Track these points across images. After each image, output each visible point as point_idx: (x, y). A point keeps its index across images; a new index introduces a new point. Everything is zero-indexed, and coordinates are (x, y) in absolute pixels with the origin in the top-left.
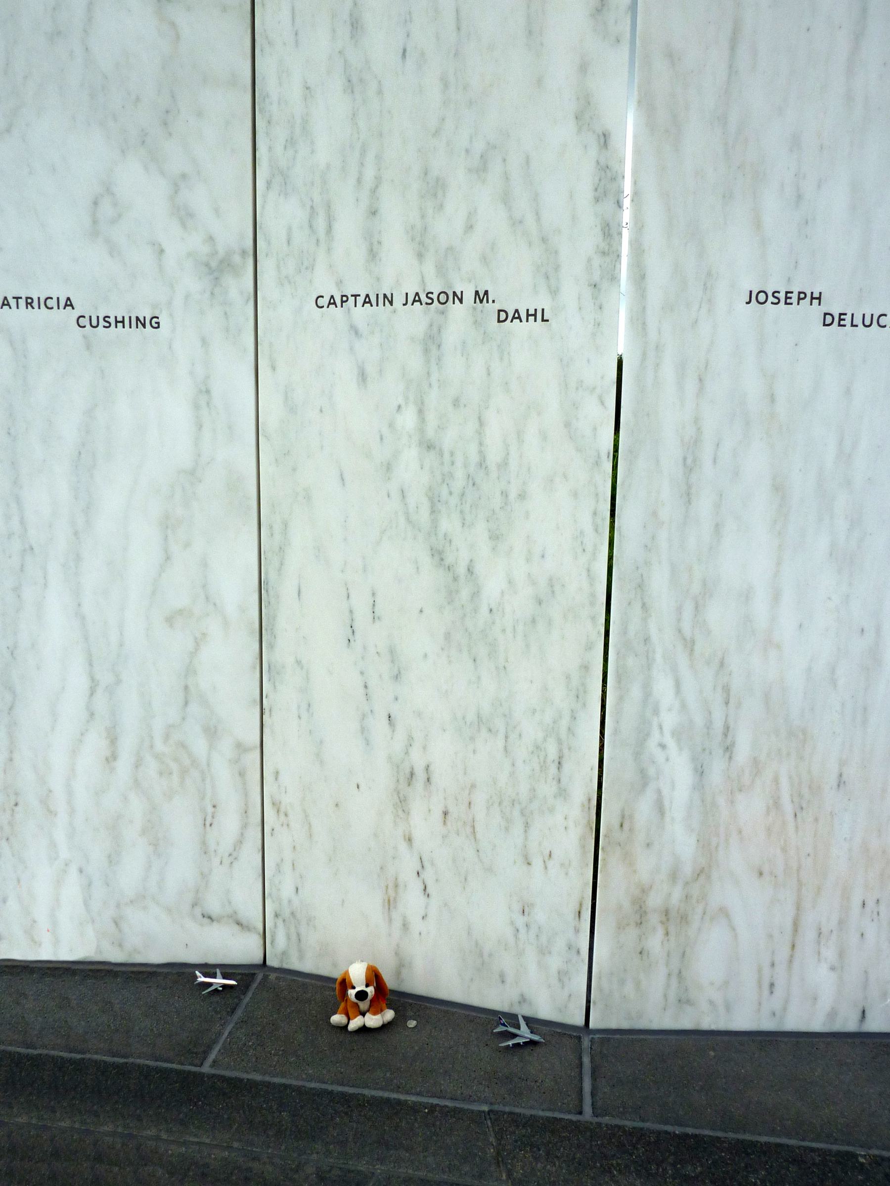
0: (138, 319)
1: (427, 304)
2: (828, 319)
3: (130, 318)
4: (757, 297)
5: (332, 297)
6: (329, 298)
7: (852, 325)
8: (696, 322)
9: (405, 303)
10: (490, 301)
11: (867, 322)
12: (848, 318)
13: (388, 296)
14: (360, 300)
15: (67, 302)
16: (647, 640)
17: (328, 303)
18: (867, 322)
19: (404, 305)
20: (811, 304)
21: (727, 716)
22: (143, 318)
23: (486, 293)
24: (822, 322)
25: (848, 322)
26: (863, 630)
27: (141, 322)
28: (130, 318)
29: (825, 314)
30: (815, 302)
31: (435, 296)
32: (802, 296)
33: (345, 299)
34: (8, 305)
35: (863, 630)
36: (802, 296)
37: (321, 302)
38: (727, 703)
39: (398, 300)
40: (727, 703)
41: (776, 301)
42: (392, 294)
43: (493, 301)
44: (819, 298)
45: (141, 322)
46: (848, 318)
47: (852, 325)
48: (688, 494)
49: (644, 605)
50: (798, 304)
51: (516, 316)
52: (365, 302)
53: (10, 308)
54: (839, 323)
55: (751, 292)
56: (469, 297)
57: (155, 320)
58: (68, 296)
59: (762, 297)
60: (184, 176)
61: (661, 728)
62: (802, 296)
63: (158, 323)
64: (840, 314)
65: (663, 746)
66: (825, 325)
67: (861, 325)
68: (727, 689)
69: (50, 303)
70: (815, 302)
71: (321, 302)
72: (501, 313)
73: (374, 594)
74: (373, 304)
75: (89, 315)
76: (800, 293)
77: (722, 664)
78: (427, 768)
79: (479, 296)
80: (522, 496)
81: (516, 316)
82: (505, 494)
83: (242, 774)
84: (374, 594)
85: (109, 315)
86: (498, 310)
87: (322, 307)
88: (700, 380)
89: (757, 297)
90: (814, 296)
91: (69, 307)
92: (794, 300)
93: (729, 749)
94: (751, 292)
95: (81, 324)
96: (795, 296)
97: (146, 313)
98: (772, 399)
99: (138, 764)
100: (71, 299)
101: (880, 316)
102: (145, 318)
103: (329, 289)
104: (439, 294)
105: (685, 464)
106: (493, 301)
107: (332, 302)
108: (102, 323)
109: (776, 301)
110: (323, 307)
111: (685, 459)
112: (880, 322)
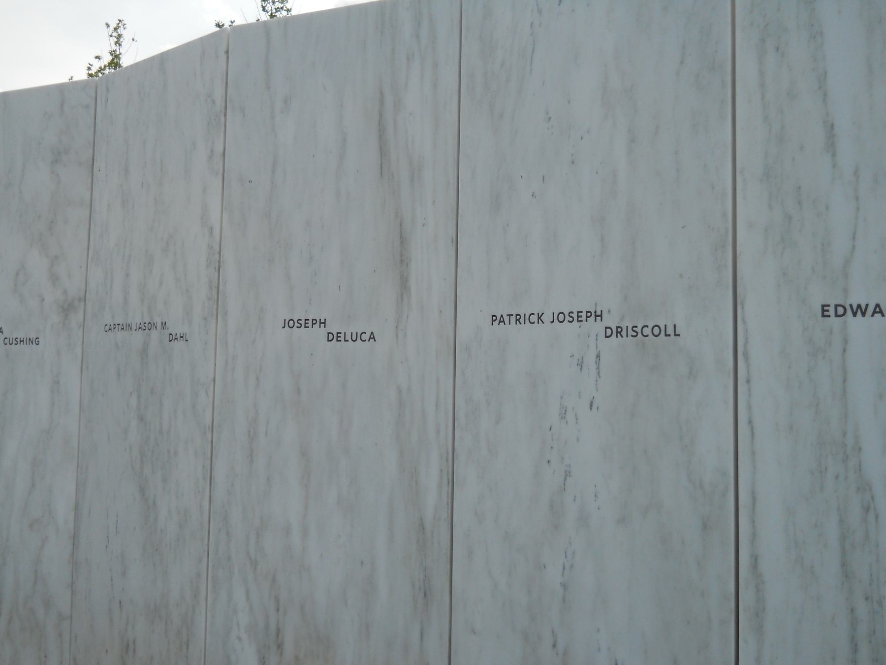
0: (30, 339)
1: (632, 336)
2: (332, 337)
3: (27, 338)
4: (289, 324)
7: (345, 341)
8: (254, 341)
9: (552, 321)
11: (354, 339)
12: (342, 335)
14: (120, 327)
15: (875, 309)
16: (229, 558)
17: (311, 324)
18: (354, 339)
19: (552, 322)
21: (278, 621)
22: (626, 328)
24: (604, 335)
25: (342, 338)
26: (362, 562)
27: (31, 341)
28: (27, 338)
29: (606, 328)
30: (599, 318)
31: (639, 330)
32: (314, 322)
33: (494, 318)
34: (503, 321)
35: (362, 562)
36: (314, 322)
38: (278, 610)
39: (547, 318)
40: (278, 610)
41: (571, 319)
42: (525, 314)
44: (324, 323)
45: (31, 341)
46: (342, 335)
47: (345, 341)
48: (251, 456)
49: (228, 533)
50: (587, 321)
53: (505, 324)
54: (337, 339)
55: (285, 320)
56: (159, 325)
58: (850, 304)
59: (291, 323)
60: (56, 257)
61: (238, 624)
62: (589, 314)
64: (338, 333)
65: (239, 639)
66: (328, 341)
67: (8, 344)
68: (277, 599)
69: (647, 331)
70: (599, 318)
72: (607, 329)
73: (117, 516)
76: (313, 320)
77: (274, 580)
78: (134, 641)
80: (176, 453)
82: (169, 451)
83: (60, 636)
84: (117, 516)
87: (534, 323)
88: (257, 379)
89: (289, 324)
90: (321, 322)
92: (310, 324)
93: (280, 646)
94: (285, 320)
96: (310, 322)
97: (33, 336)
98: (299, 391)
99: (10, 621)
101: (362, 333)
103: (109, 321)
104: (293, 326)
105: (249, 435)
108: (631, 332)
109: (571, 319)
110: (365, 340)
111: (249, 431)
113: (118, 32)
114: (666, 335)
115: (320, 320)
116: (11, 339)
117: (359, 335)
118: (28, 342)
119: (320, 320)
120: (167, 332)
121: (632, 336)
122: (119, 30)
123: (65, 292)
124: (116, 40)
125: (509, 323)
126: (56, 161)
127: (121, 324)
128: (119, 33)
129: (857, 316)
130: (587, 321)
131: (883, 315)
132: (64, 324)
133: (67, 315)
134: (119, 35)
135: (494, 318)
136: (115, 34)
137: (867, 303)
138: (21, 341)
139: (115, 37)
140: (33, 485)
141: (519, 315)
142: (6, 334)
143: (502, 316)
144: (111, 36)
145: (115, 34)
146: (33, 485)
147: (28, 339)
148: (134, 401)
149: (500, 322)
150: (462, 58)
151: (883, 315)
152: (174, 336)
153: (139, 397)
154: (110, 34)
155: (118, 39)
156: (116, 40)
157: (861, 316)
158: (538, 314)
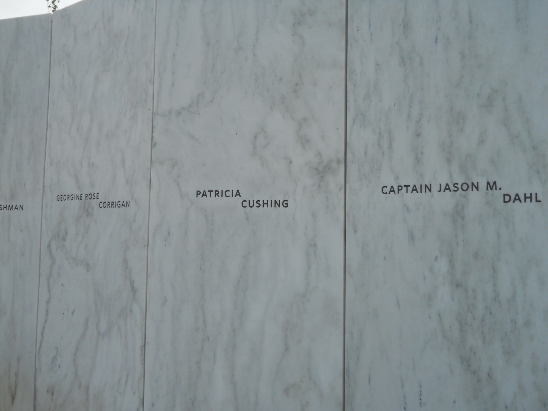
1: (454, 191)
3: (271, 201)
5: (392, 187)
6: (390, 187)
9: (439, 190)
10: (498, 188)
11: (251, 205)
13: (428, 186)
14: (410, 189)
15: (516, 197)
18: (251, 205)
19: (439, 191)
20: (197, 197)
23: (495, 183)
27: (277, 204)
30: (265, 202)
34: (206, 195)
37: (385, 190)
39: (435, 188)
42: (222, 191)
43: (500, 189)
45: (277, 204)
51: (392, 190)
52: (413, 190)
53: (207, 197)
56: (483, 186)
57: (285, 202)
60: (305, 120)
63: (287, 204)
67: (103, 207)
69: (228, 194)
71: (385, 190)
74: (418, 191)
75: (123, 201)
79: (21, 208)
81: (392, 190)
82: (514, 322)
85: (72, 194)
86: (288, 204)
87: (246, 207)
91: (415, 191)
94: (253, 201)
95: (384, 192)
97: (280, 198)
100: (394, 187)
102: (280, 201)
103: (390, 182)
106: (500, 189)
107: (392, 190)
112: (243, 205)
113: (54, 4)
114: (537, 201)
115: (267, 207)
116: (75, 199)
117: (117, 204)
118: (76, 197)
119: (267, 207)
120: (498, 194)
121: (454, 191)
122: (55, 3)
123: (319, 154)
124: (53, 9)
125: (210, 196)
126: (299, 24)
127: (412, 186)
128: (55, 5)
129: (486, 183)
130: (398, 193)
131: (240, 197)
132: (319, 186)
133: (322, 177)
134: (55, 6)
135: (198, 193)
136: (52, 5)
137: (541, 201)
138: (4, 207)
139: (52, 7)
140: (287, 349)
141: (218, 191)
142: (244, 197)
143: (204, 191)
144: (50, 7)
145: (52, 5)
146: (287, 349)
147: (273, 202)
148: (443, 266)
149: (203, 195)
150: (348, 9)
151: (240, 197)
152: (107, 204)
153: (451, 262)
154: (49, 6)
155: (54, 8)
156: (53, 9)
157: (429, 192)
158: (496, 189)
